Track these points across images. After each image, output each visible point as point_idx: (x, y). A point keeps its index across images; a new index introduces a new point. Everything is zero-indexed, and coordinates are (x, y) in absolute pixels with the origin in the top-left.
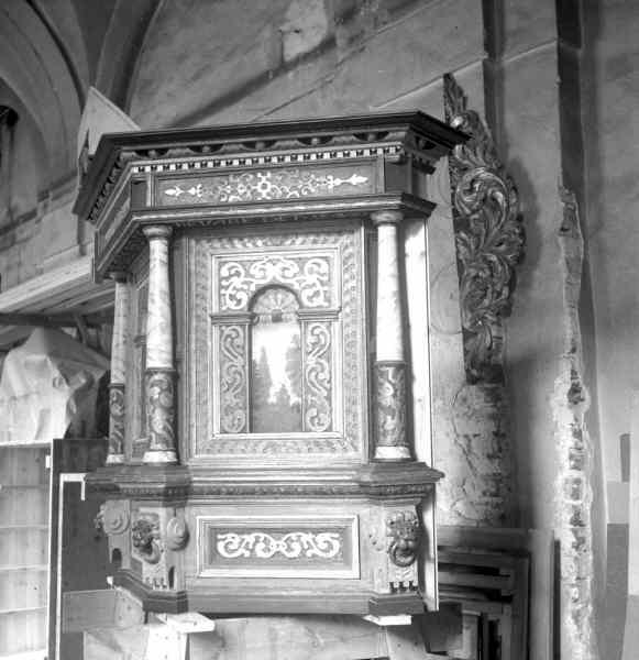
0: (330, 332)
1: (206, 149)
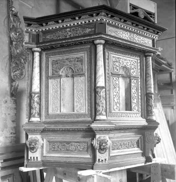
0: (119, 80)
1: (146, 29)
